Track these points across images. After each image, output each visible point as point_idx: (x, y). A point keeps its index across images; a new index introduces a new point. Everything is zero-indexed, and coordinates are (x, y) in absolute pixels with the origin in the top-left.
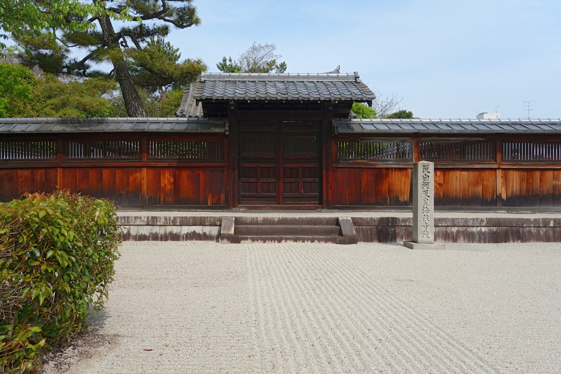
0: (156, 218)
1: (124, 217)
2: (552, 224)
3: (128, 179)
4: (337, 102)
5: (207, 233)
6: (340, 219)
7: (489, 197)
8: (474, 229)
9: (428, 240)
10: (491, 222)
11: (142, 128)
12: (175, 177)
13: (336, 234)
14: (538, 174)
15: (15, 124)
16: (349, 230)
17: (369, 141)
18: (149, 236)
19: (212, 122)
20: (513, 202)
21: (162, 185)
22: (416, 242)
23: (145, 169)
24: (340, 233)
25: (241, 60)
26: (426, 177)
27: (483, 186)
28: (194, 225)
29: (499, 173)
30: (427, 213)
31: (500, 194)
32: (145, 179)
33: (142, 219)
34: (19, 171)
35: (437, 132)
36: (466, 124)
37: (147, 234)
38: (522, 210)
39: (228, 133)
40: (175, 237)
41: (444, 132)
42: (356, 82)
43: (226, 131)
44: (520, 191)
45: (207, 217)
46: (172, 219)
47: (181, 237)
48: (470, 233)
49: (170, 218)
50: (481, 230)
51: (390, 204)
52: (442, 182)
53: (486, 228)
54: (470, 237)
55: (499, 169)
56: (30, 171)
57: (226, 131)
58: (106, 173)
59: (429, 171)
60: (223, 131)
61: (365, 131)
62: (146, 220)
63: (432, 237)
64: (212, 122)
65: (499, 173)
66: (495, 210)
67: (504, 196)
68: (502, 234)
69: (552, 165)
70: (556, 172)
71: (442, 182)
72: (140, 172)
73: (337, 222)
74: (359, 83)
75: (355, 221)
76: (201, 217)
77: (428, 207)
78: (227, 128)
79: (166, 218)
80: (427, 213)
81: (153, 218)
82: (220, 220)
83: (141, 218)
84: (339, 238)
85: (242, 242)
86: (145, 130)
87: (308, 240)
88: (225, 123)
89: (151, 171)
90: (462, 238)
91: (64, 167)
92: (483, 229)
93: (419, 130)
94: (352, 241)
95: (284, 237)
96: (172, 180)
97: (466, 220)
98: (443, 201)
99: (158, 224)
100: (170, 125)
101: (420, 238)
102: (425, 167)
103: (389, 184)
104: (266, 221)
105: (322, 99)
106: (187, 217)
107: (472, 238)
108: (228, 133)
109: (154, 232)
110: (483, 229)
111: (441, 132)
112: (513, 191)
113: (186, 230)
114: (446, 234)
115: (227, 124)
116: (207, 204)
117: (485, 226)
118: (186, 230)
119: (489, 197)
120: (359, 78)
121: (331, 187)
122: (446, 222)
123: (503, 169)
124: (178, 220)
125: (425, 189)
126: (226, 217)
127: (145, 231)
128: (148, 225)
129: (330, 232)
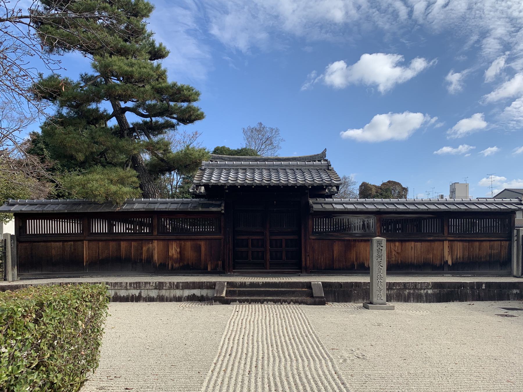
0: (163, 283)
1: (136, 283)
2: (484, 287)
3: (142, 248)
4: (310, 187)
5: (205, 295)
6: (312, 283)
7: (438, 263)
8: (422, 291)
9: (381, 301)
10: (436, 285)
11: (153, 207)
12: (180, 248)
13: (308, 296)
14: (477, 244)
15: (49, 205)
16: (319, 292)
17: (340, 218)
18: (157, 298)
19: (210, 202)
20: (457, 267)
21: (170, 254)
22: (371, 303)
23: (156, 242)
24: (311, 295)
25: (512, 26)
26: (379, 251)
27: (433, 254)
28: (194, 288)
29: (446, 244)
30: (381, 278)
31: (447, 261)
32: (156, 250)
33: (151, 284)
34: (52, 243)
35: (395, 210)
36: (419, 204)
37: (155, 297)
38: (465, 274)
39: (223, 212)
40: (179, 299)
41: (401, 210)
42: (328, 169)
43: (222, 210)
44: (463, 258)
45: (205, 282)
46: (175, 284)
47: (183, 299)
48: (419, 295)
49: (174, 283)
50: (427, 292)
51: (357, 270)
52: (400, 251)
53: (431, 290)
54: (419, 299)
55: (446, 240)
56: (61, 243)
57: (222, 210)
58: (123, 244)
59: (382, 245)
60: (219, 209)
61: (336, 210)
62: (154, 285)
63: (384, 298)
64: (210, 202)
65: (446, 244)
66: (442, 275)
67: (450, 262)
68: (446, 294)
69: (488, 237)
70: (492, 243)
71: (400, 251)
72: (152, 243)
73: (309, 285)
74: (330, 170)
75: (325, 285)
76: (199, 282)
77: (382, 275)
78: (223, 208)
79: (170, 283)
80: (381, 278)
81: (160, 283)
82: (214, 284)
83: (150, 283)
84: (309, 299)
85: (231, 303)
86: (156, 210)
87: (285, 301)
88: (221, 203)
89: (161, 243)
90: (412, 299)
91: (88, 240)
92: (430, 292)
93: (380, 209)
94: (321, 302)
95: (266, 298)
96: (178, 250)
97: (415, 284)
98: (393, 268)
99: (164, 288)
100: (176, 205)
101: (375, 300)
102: (379, 243)
103: (356, 253)
104: (252, 285)
105: (298, 185)
106: (187, 282)
107: (420, 299)
108: (223, 212)
109: (161, 295)
110: (430, 292)
111: (398, 210)
112: (457, 259)
113: (187, 293)
114: (400, 294)
115: (223, 205)
116: (207, 270)
117: (431, 289)
118: (187, 293)
119: (438, 263)
120: (330, 165)
121: (309, 255)
122: (399, 286)
123: (449, 240)
124: (181, 285)
125: (379, 260)
126: (220, 282)
127: (154, 294)
128: (156, 289)
129: (302, 294)
